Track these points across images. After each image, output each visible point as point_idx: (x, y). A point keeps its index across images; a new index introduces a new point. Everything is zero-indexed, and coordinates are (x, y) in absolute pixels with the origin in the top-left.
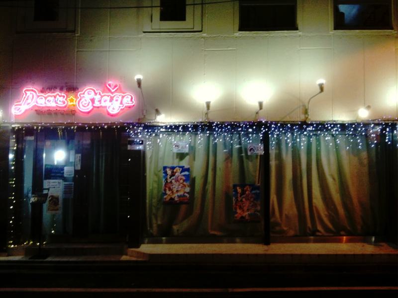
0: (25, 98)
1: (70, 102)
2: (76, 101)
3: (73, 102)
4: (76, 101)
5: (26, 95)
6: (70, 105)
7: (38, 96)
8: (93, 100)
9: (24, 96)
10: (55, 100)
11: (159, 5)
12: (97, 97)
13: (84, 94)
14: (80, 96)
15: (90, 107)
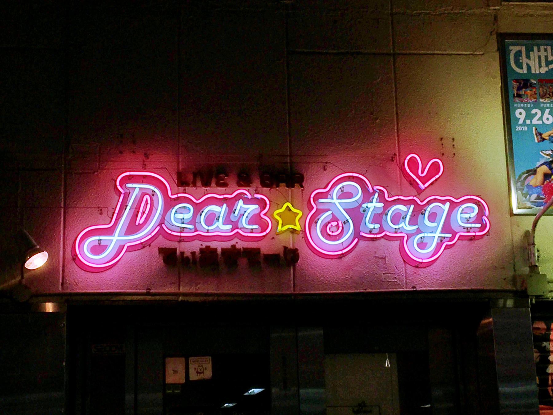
8: (356, 214)
10: (226, 217)
11: (194, 376)
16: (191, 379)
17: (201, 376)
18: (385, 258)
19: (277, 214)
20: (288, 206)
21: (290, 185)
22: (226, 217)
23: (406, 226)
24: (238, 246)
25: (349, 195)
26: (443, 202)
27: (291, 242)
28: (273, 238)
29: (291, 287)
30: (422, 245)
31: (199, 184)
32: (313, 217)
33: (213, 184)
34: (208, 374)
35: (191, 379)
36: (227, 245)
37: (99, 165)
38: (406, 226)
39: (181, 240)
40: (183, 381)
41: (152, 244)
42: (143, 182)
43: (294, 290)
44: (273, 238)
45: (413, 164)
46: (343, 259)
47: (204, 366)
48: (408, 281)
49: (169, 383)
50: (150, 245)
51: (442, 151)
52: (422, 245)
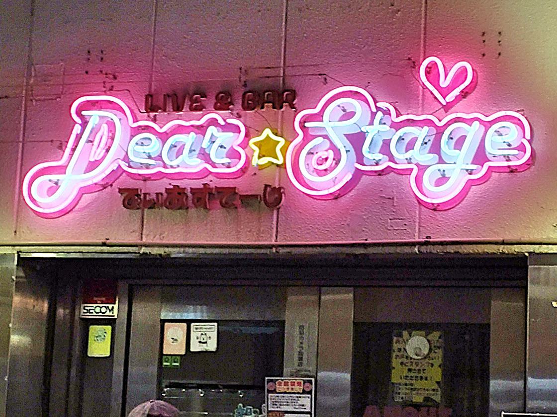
0: (79, 137)
1: (268, 137)
2: (284, 150)
3: (281, 383)
4: (284, 150)
5: (84, 124)
6: (260, 168)
7: (136, 131)
8: (357, 140)
9: (77, 129)
10: (205, 147)
11: (195, 347)
12: (377, 131)
13: (319, 117)
14: (303, 127)
15: (342, 174)
16: (192, 350)
17: (203, 348)
18: (393, 199)
19: (255, 144)
20: (397, 116)
21: (278, 105)
22: (205, 147)
23: (421, 155)
24: (212, 185)
25: (348, 115)
26: (469, 122)
27: (277, 179)
28: (255, 174)
29: (238, 242)
30: (442, 180)
31: (169, 107)
32: (508, 117)
33: (186, 107)
34: (212, 346)
35: (192, 350)
36: (198, 184)
37: (63, 89)
38: (421, 155)
39: (146, 178)
40: (183, 353)
41: (114, 184)
42: (101, 108)
43: (276, 241)
44: (255, 174)
45: (431, 71)
46: (339, 199)
47: (209, 334)
48: (421, 228)
49: (215, 346)
50: (111, 185)
51: (483, 51)
52: (442, 180)
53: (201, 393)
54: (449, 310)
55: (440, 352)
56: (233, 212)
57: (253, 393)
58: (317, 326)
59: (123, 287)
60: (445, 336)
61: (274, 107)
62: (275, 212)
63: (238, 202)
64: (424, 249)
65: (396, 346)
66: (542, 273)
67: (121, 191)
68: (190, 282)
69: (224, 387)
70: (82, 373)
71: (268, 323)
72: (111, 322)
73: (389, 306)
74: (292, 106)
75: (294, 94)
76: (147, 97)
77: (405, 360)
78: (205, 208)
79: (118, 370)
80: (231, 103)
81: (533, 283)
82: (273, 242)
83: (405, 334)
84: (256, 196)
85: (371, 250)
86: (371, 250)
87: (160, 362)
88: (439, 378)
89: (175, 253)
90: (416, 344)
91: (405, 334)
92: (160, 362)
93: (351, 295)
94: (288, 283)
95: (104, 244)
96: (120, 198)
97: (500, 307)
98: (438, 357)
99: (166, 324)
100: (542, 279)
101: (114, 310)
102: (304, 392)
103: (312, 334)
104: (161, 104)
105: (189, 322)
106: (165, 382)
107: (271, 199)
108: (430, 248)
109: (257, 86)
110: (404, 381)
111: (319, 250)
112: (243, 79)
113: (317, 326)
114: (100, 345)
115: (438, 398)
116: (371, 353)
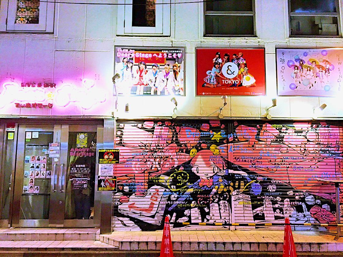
21: (52, 87)
31: (27, 86)
33: (31, 86)
34: (37, 137)
53: (35, 147)
54: (165, 113)
55: (87, 137)
56: (41, 108)
57: (46, 146)
58: (60, 134)
59: (17, 124)
60: (88, 134)
61: (51, 87)
62: (51, 109)
63: (43, 107)
64: (83, 117)
65: (77, 136)
66: (107, 122)
67: (15, 104)
68: (25, 123)
69: (40, 145)
70: (7, 143)
71: (50, 132)
72: (14, 132)
73: (75, 129)
74: (55, 87)
75: (55, 85)
76: (22, 84)
77: (79, 139)
78: (35, 108)
79: (15, 143)
80: (41, 86)
81: (105, 124)
82: (51, 115)
83: (80, 134)
84: (47, 106)
85: (72, 117)
86: (72, 117)
87: (25, 140)
88: (86, 143)
89: (28, 117)
90: (82, 136)
91: (80, 134)
92: (25, 140)
93: (68, 127)
94: (180, 157)
95: (11, 115)
96: (15, 105)
97: (99, 129)
98: (86, 138)
99: (27, 132)
100: (107, 123)
101: (15, 129)
102: (58, 146)
103: (59, 134)
104: (25, 85)
105: (32, 132)
106: (26, 145)
107: (50, 106)
108: (84, 117)
109: (47, 82)
110: (79, 143)
111: (61, 117)
112: (44, 81)
113: (60, 134)
114: (11, 137)
115: (86, 147)
116: (73, 138)
